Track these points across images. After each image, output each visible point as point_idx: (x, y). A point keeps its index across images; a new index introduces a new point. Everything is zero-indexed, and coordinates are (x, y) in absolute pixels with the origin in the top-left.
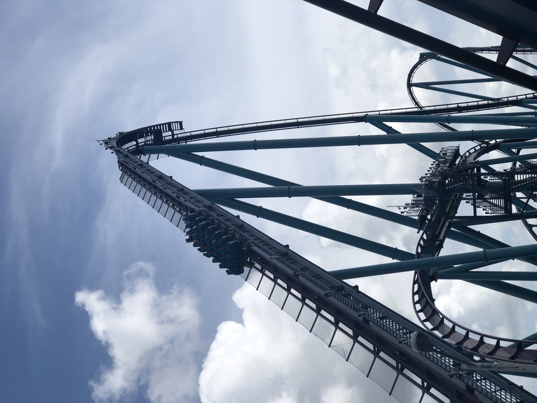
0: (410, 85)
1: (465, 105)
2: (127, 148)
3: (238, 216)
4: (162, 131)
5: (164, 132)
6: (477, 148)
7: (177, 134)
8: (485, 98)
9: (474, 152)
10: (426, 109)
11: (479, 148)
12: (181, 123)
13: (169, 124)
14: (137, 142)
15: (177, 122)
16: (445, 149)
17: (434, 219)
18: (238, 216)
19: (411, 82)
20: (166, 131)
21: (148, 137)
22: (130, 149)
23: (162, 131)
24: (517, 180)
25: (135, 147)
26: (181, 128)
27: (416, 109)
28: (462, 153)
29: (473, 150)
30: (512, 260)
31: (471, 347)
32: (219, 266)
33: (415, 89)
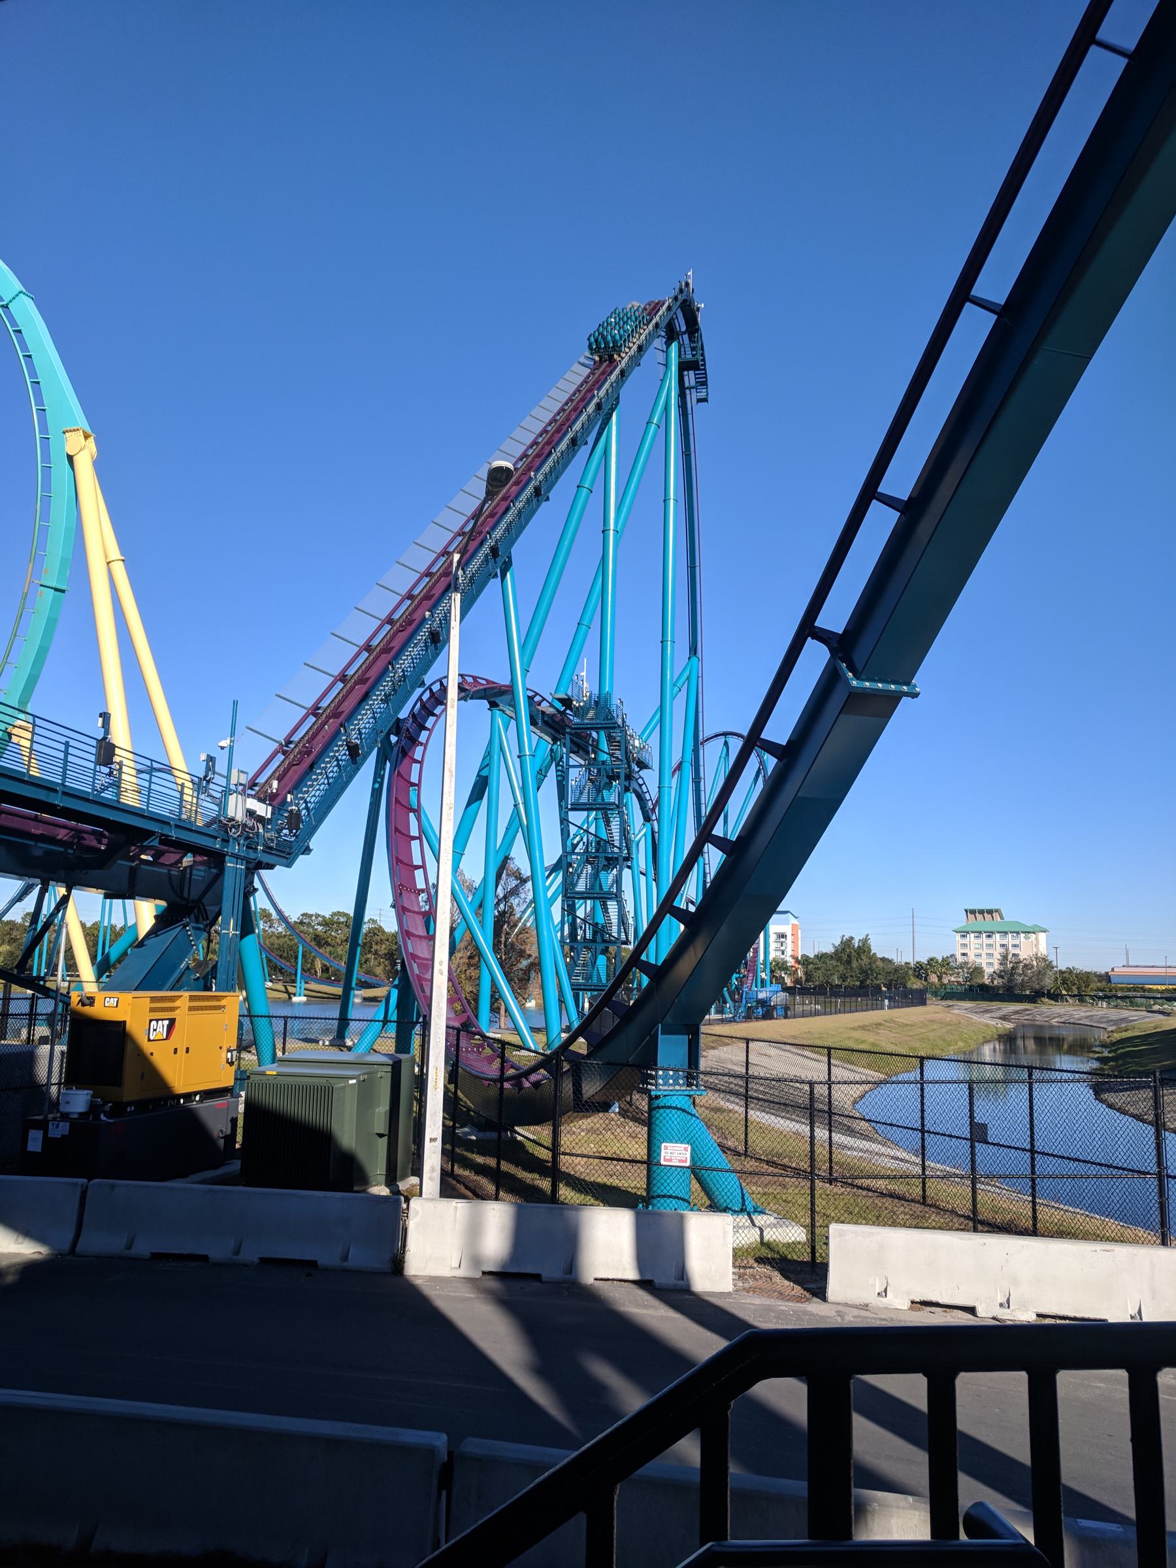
0: (725, 734)
2: (677, 317)
5: (695, 374)
6: (647, 795)
8: (779, 1048)
9: (642, 791)
12: (705, 400)
13: (705, 384)
14: (684, 333)
15: (707, 395)
16: (1099, 1239)
17: (1058, 1022)
19: (692, 909)
20: (696, 378)
22: (676, 321)
24: (187, 897)
25: (678, 329)
26: (699, 401)
27: (701, 738)
28: (643, 773)
29: (645, 790)
33: (722, 740)
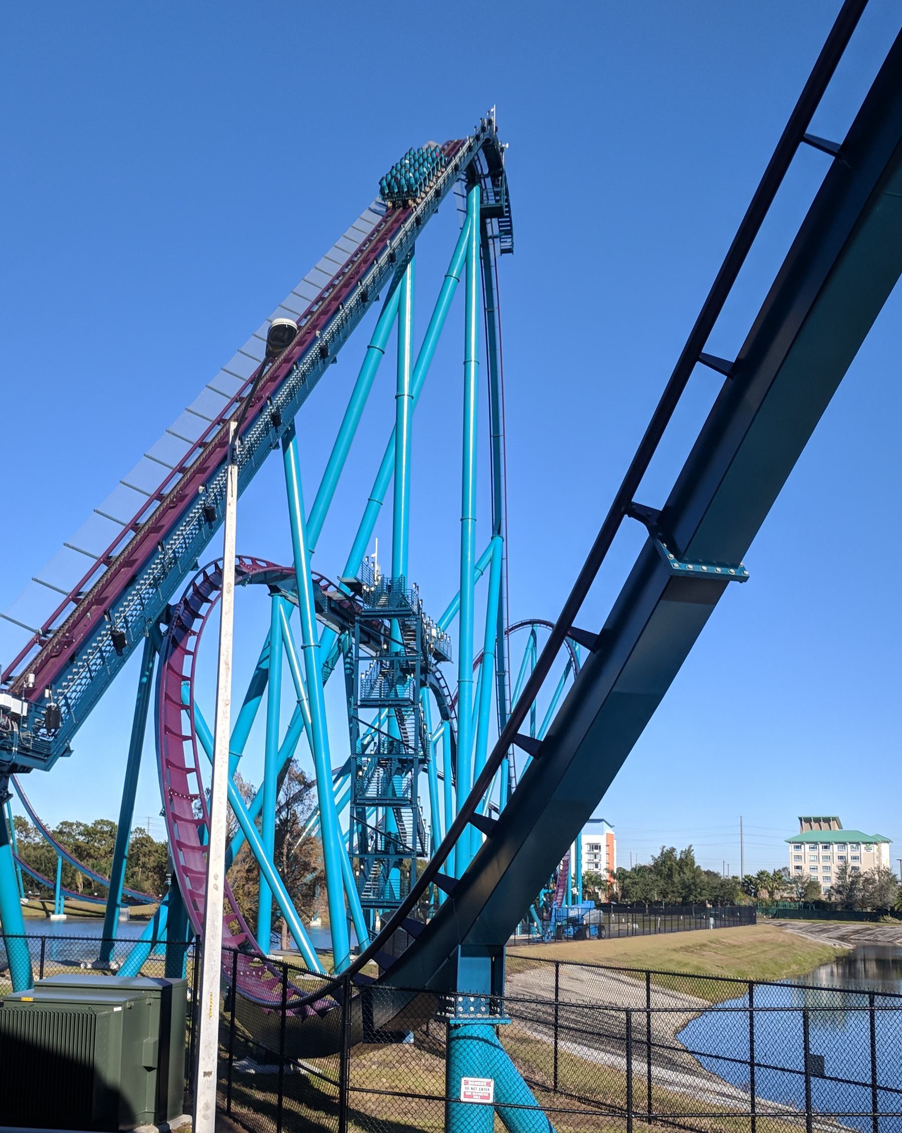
0: (532, 622)
1: (507, 683)
3: (378, 299)
4: (500, 220)
5: (499, 222)
6: (445, 690)
7: (491, 222)
9: (440, 686)
10: (506, 642)
11: (446, 693)
12: (510, 251)
14: (487, 176)
18: (378, 299)
20: (500, 227)
21: (493, 194)
22: (478, 163)
23: (500, 220)
26: (504, 251)
27: (505, 626)
28: (442, 666)
29: (443, 685)
30: (60, 759)
31: (732, 584)
32: (668, 855)
33: (528, 628)
